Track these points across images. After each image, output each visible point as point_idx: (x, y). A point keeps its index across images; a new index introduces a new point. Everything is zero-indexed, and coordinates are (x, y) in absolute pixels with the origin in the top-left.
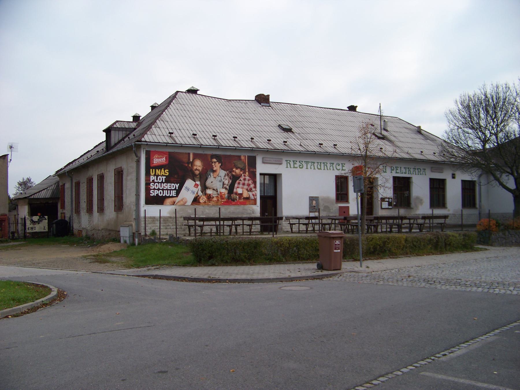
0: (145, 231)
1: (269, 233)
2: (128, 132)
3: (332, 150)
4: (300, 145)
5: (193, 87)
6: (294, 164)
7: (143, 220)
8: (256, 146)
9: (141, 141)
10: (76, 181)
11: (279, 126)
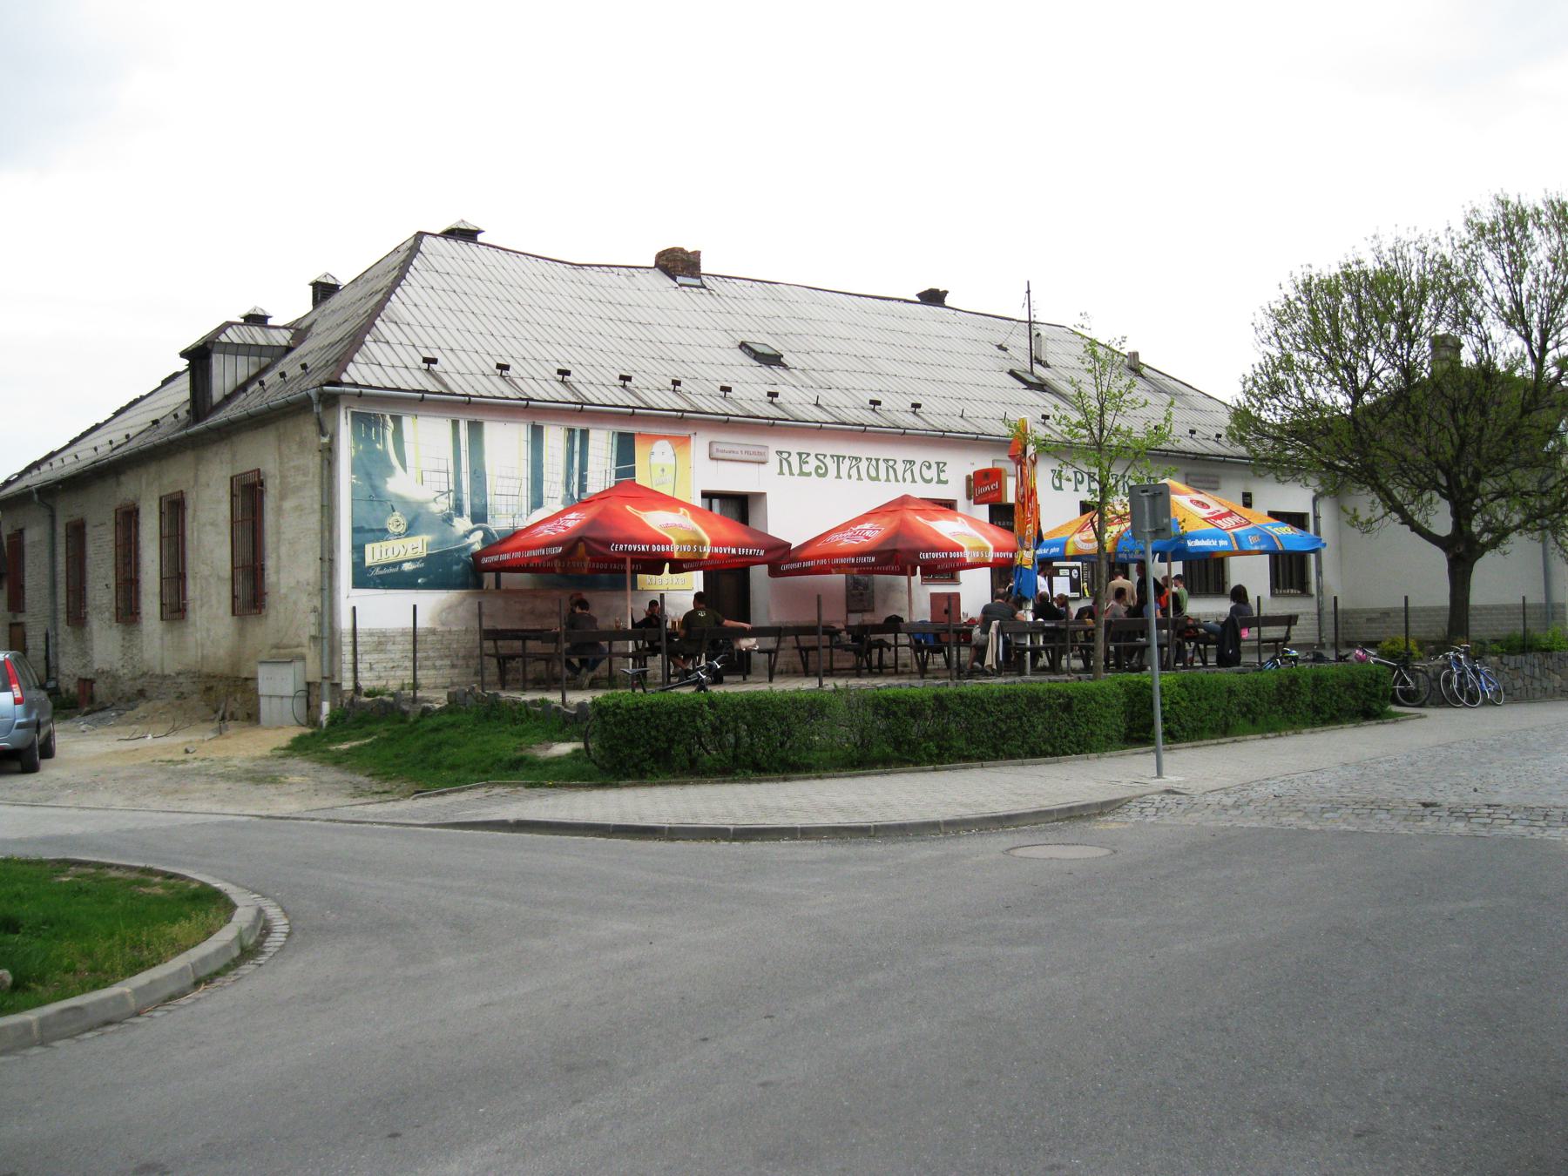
0: (356, 677)
1: (744, 679)
2: (266, 360)
3: (909, 420)
4: (817, 405)
5: (463, 221)
6: (802, 462)
7: (347, 639)
8: (691, 405)
9: (339, 383)
10: (68, 520)
11: (740, 347)
